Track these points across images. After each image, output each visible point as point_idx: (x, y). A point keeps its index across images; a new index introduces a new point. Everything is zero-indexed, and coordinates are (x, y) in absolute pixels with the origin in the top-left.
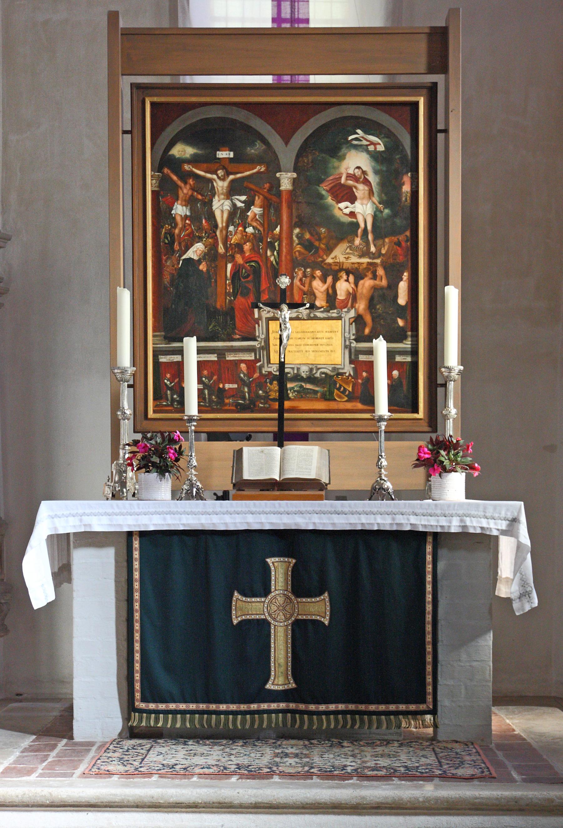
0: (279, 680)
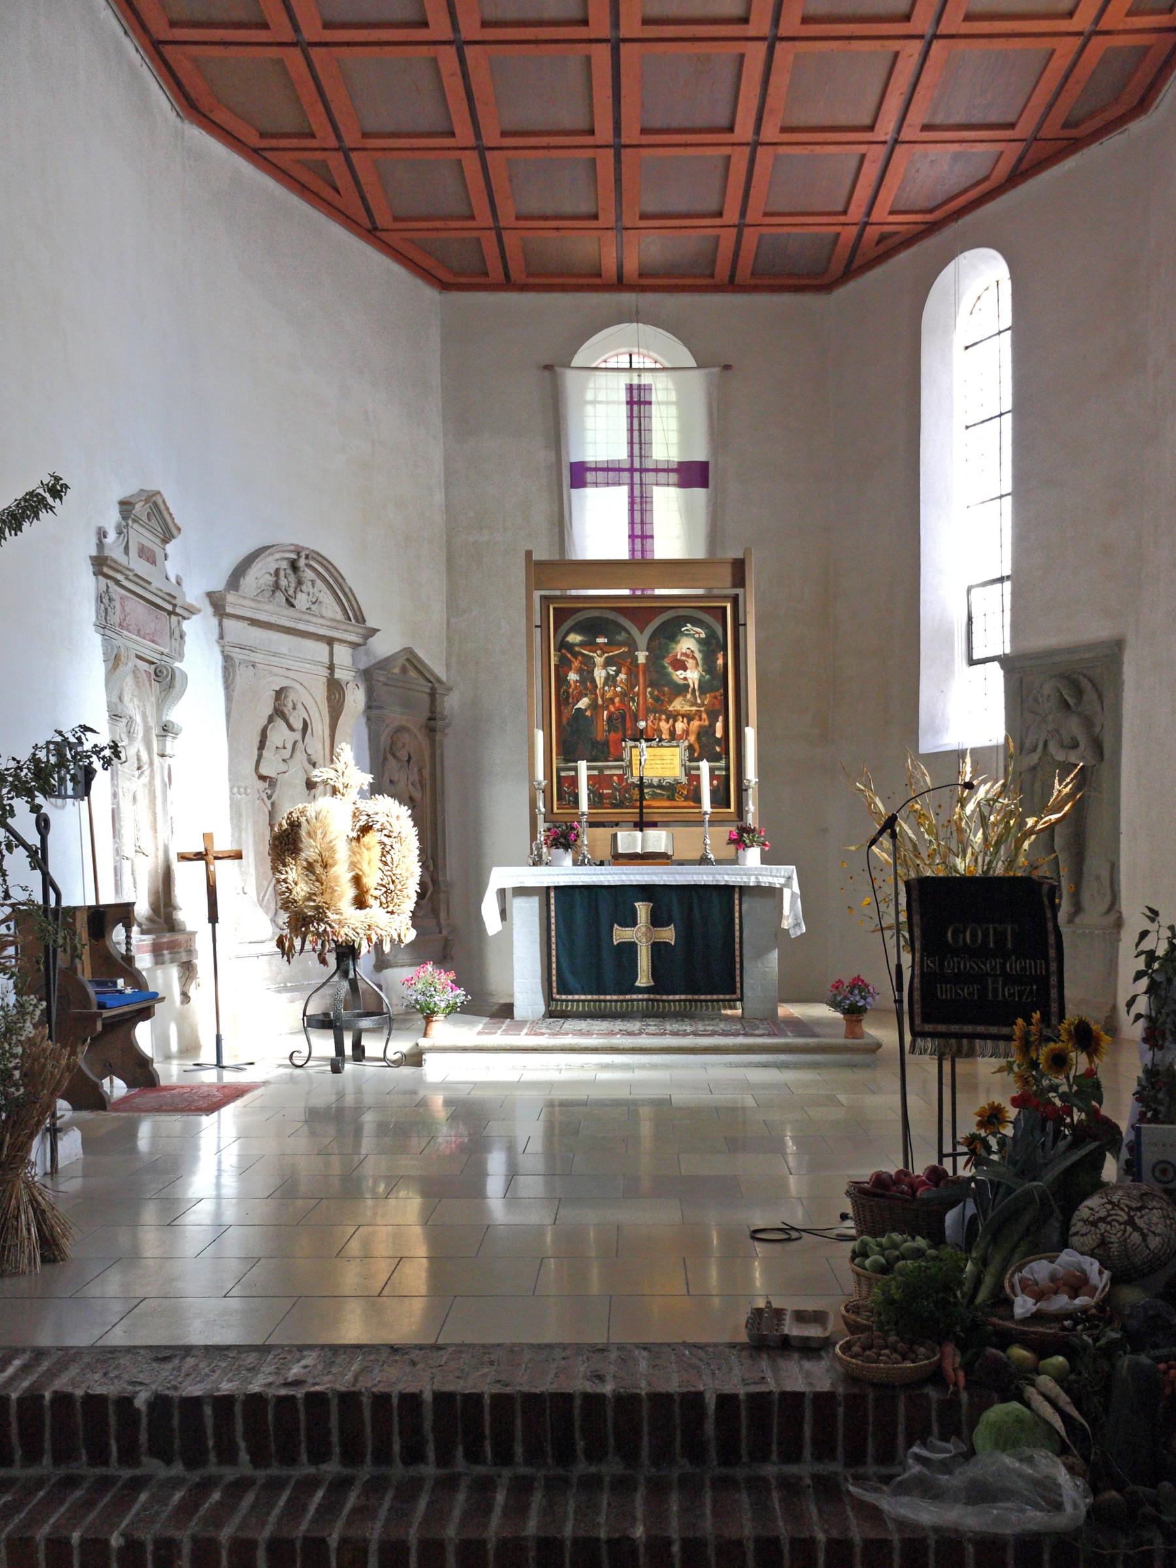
0: (643, 979)
